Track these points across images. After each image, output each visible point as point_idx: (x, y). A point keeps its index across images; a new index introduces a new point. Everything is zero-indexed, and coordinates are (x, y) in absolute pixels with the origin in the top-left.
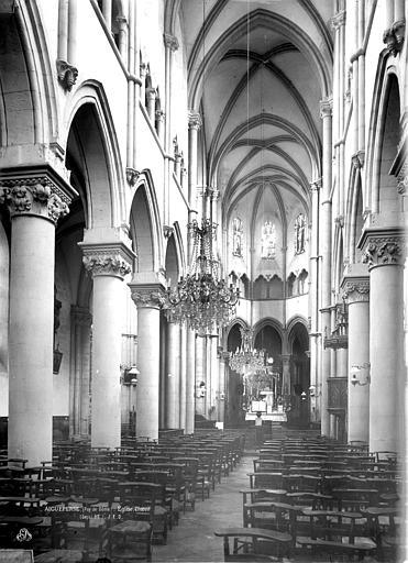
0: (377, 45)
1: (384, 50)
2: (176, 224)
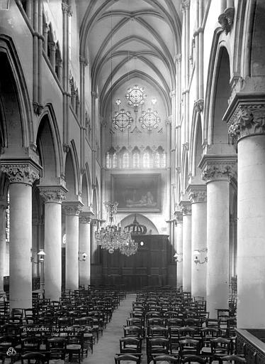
0: (213, 23)
1: (220, 28)
2: (73, 142)
